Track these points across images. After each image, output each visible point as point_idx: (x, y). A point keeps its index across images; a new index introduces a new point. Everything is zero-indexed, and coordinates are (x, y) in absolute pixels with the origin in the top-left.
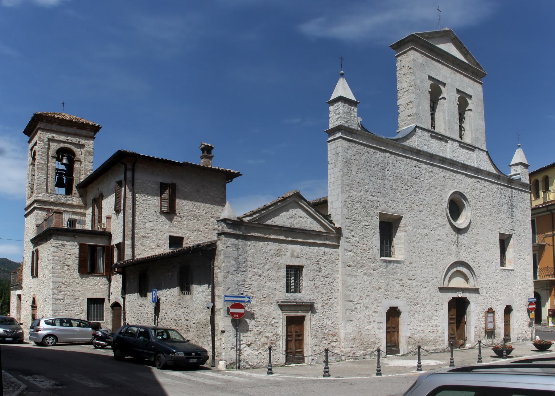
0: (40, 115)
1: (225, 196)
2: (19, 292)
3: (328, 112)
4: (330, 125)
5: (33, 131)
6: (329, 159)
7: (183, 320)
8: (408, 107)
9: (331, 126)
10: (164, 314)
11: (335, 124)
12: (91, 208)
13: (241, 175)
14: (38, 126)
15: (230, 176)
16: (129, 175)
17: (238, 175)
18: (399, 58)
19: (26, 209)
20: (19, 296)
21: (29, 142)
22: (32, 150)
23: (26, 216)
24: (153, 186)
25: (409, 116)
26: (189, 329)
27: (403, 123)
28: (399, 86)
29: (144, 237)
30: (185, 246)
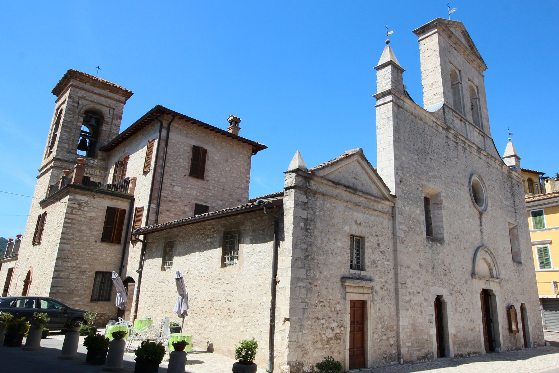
0: (76, 72)
1: (250, 167)
2: (11, 265)
3: (375, 78)
4: (378, 90)
5: (62, 90)
6: (377, 124)
7: (223, 301)
8: (433, 87)
9: (379, 91)
10: (194, 292)
11: (384, 88)
12: (145, 148)
13: (267, 147)
14: (71, 83)
15: (256, 148)
16: (164, 133)
17: (264, 147)
18: (422, 42)
19: (40, 171)
20: (11, 271)
21: (56, 102)
22: (58, 109)
23: (38, 177)
24: (185, 148)
25: (435, 95)
26: (232, 314)
27: (429, 102)
28: (422, 68)
29: (170, 201)
30: (27, 296)
